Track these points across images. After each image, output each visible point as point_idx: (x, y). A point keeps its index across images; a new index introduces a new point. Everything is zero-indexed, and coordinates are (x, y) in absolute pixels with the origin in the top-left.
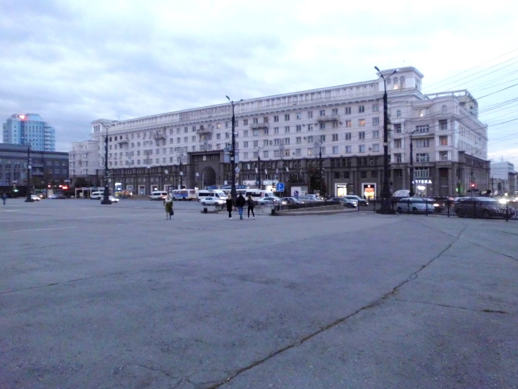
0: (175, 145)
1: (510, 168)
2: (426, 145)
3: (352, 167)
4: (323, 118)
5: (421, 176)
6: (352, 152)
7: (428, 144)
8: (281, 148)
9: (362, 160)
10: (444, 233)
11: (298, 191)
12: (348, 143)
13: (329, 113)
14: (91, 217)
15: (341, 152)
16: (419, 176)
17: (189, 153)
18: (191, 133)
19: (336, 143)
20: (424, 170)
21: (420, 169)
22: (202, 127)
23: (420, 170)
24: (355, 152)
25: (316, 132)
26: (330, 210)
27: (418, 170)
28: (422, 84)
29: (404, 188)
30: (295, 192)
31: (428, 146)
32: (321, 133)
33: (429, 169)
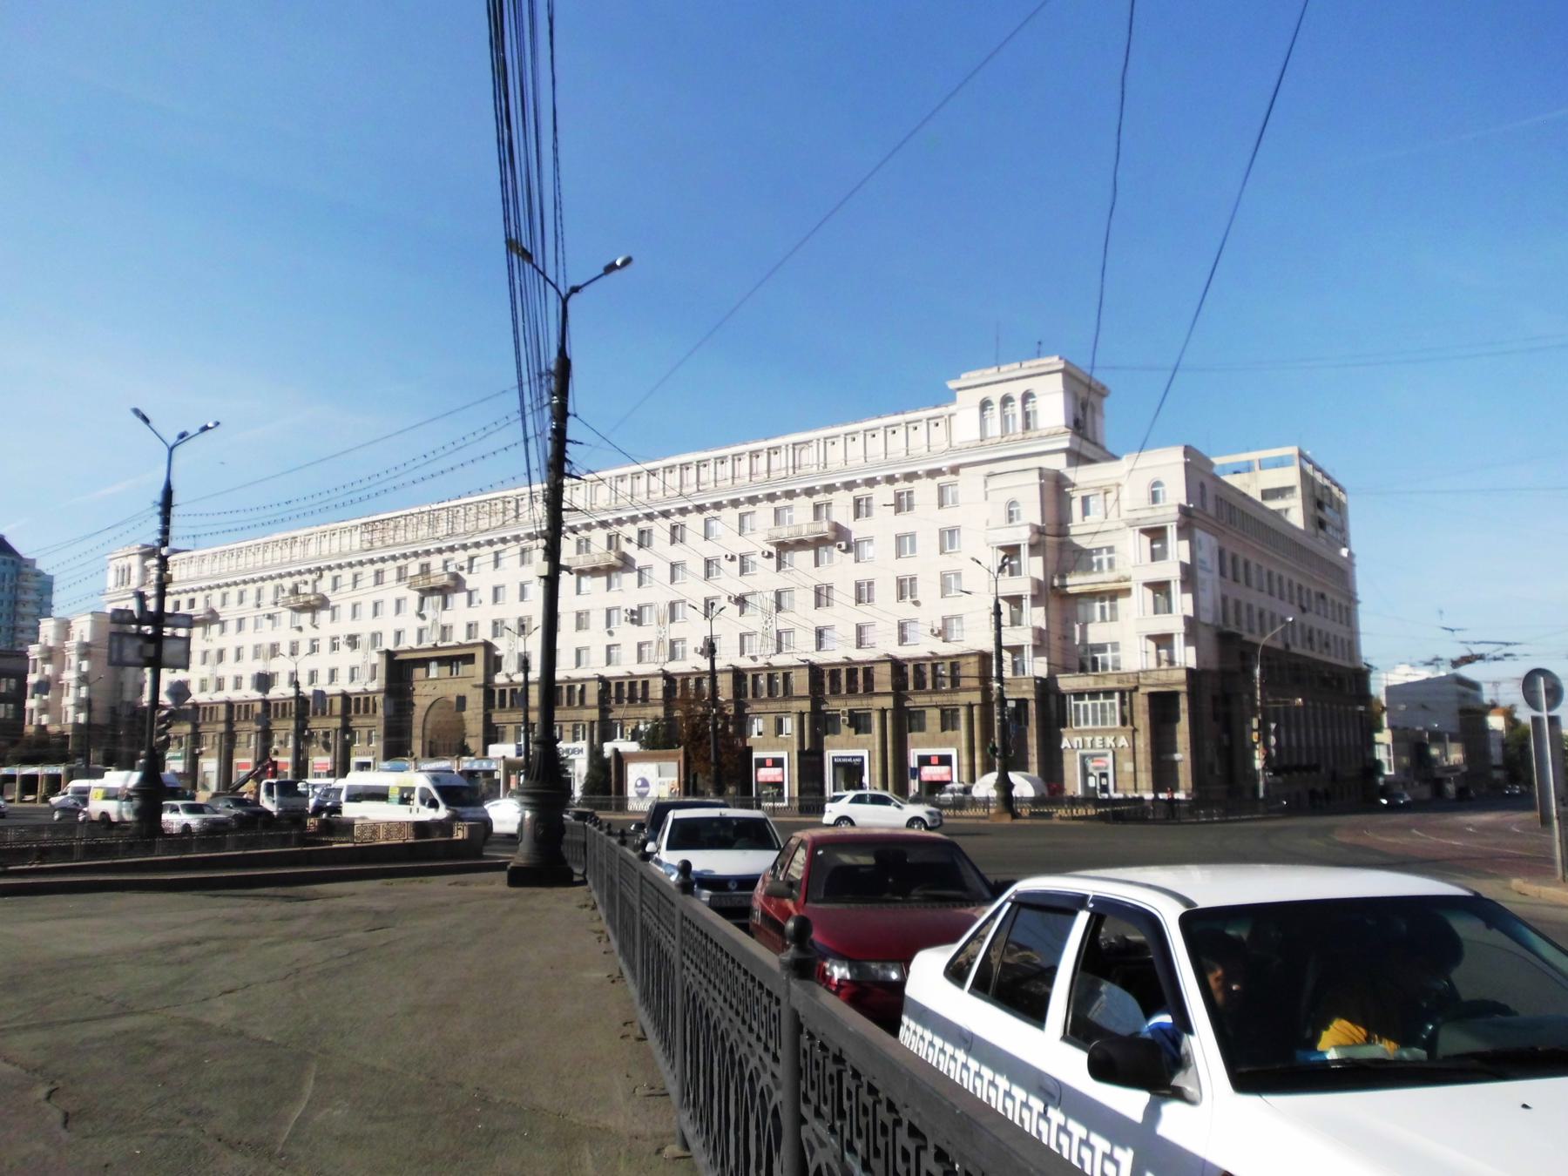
0: (345, 627)
1: (1464, 695)
2: (1108, 616)
3: (877, 694)
4: (786, 533)
5: (1095, 722)
6: (1122, 666)
7: (1113, 608)
8: (660, 632)
9: (910, 669)
10: (143, 1012)
11: (648, 778)
12: (862, 614)
13: (801, 519)
14: (1443, 841)
15: (837, 652)
16: (1086, 721)
17: (389, 655)
18: (393, 590)
19: (822, 617)
20: (1101, 700)
21: (1090, 699)
22: (425, 570)
23: (1087, 702)
24: (884, 644)
25: (765, 577)
26: (1560, 831)
27: (1081, 703)
28: (1102, 415)
29: (390, 740)
30: (639, 783)
31: (1114, 619)
32: (780, 581)
33: (1117, 695)
